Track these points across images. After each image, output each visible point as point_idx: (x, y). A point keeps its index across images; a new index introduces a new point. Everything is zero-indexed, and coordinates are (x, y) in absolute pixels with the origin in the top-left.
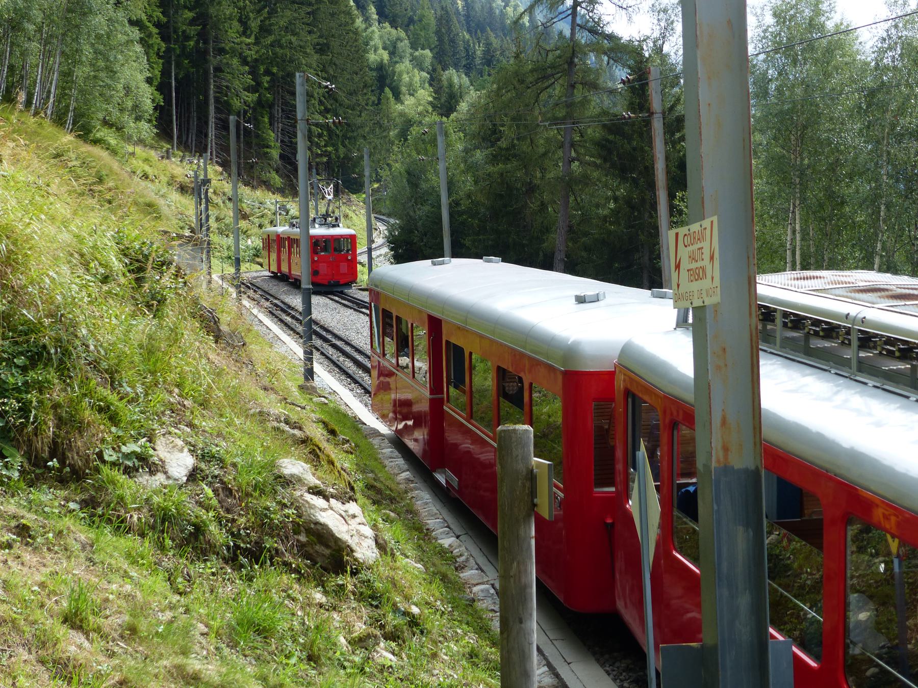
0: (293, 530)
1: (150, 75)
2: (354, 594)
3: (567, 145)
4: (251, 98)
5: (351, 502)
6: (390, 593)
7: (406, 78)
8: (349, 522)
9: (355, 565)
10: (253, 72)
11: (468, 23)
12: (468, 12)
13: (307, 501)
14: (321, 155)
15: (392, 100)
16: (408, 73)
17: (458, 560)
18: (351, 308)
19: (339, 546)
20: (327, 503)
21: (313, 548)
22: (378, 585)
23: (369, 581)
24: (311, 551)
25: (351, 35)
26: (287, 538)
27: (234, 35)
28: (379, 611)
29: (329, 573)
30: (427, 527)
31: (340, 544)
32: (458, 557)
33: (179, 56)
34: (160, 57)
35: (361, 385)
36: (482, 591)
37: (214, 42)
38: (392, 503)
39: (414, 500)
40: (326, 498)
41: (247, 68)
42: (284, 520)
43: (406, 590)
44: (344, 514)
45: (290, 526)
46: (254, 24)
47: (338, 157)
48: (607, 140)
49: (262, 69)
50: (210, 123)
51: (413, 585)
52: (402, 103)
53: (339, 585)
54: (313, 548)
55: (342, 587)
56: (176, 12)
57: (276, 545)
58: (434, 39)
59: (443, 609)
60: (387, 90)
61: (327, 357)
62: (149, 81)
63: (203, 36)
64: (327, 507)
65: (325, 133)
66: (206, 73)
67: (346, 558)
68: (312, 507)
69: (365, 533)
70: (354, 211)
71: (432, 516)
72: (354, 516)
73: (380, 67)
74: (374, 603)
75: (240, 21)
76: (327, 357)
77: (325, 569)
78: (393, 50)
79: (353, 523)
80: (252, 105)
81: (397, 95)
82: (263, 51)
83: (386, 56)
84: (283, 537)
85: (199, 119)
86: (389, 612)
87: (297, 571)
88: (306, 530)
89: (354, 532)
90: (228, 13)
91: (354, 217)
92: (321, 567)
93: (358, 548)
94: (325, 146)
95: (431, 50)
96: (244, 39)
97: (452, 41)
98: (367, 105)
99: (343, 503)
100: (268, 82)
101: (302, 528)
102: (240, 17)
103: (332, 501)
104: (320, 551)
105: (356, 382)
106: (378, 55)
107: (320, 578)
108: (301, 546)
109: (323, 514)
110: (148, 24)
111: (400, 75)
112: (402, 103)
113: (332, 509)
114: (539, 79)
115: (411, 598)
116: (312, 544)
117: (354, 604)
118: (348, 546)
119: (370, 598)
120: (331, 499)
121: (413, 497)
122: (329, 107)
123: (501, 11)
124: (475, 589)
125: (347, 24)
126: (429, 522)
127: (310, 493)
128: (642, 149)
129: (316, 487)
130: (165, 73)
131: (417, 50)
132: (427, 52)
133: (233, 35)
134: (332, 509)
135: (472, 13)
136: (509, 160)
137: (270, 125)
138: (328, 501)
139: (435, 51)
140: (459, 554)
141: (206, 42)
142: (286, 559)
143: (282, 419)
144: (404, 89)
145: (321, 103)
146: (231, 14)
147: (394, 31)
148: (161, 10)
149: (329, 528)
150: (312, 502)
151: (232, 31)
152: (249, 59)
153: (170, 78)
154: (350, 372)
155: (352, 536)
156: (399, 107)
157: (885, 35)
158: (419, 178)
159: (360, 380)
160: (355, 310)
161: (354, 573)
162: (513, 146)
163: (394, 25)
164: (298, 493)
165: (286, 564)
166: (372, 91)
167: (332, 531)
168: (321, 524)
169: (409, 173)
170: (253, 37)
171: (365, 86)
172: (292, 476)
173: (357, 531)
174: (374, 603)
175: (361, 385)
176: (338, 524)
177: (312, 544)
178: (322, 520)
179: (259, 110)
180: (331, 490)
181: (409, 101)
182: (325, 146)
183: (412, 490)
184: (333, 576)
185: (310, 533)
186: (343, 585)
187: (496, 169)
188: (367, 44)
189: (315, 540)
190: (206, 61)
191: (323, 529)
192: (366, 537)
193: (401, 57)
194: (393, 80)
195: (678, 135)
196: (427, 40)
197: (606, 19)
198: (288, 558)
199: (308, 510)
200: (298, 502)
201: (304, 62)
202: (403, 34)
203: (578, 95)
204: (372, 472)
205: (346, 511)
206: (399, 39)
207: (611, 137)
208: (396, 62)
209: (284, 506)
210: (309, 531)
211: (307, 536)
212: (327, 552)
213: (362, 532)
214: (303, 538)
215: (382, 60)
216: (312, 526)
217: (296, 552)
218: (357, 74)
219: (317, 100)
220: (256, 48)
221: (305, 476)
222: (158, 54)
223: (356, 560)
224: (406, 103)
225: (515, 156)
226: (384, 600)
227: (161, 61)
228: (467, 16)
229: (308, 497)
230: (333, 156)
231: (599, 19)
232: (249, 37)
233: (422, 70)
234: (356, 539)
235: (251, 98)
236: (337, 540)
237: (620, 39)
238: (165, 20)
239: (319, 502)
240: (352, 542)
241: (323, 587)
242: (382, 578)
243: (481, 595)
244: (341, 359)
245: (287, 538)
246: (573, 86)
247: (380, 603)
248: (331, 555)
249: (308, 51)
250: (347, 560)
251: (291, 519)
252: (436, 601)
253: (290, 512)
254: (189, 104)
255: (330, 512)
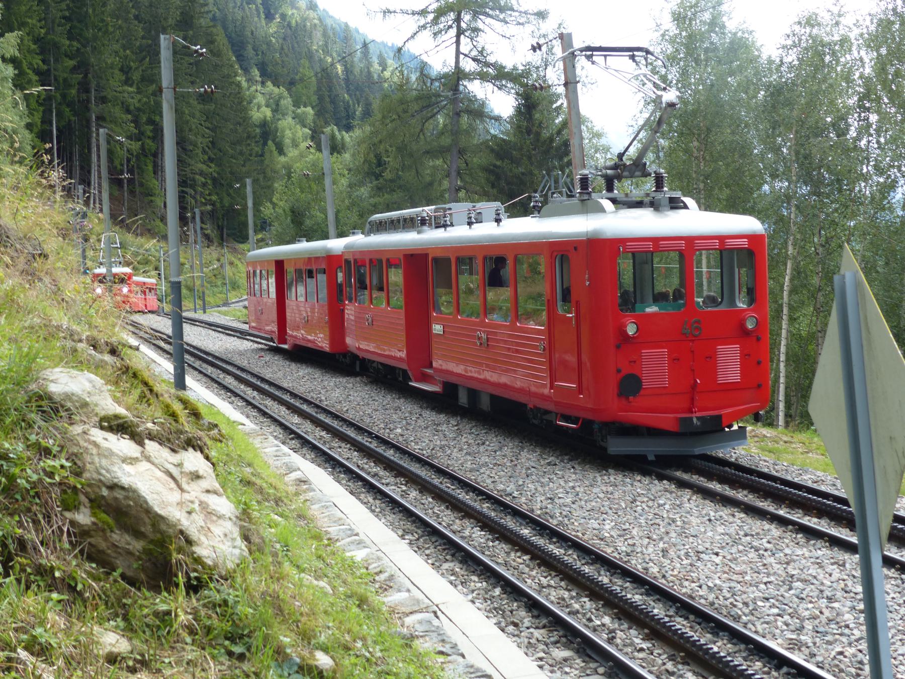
0: (63, 501)
1: (29, 121)
2: (192, 632)
3: (454, 174)
4: (135, 146)
5: (191, 450)
6: (269, 626)
7: (288, 133)
8: (185, 486)
9: (195, 570)
10: (136, 121)
11: (347, 86)
12: (347, 76)
13: (95, 444)
14: (205, 204)
15: (275, 153)
16: (290, 129)
17: (377, 578)
18: (234, 336)
19: (162, 533)
20: (139, 448)
21: (106, 539)
22: (245, 610)
23: (225, 602)
24: (103, 545)
25: (234, 86)
26: (48, 517)
27: (116, 84)
28: (246, 666)
29: (139, 589)
30: (328, 536)
31: (163, 527)
32: (377, 574)
33: (60, 104)
34: (40, 104)
35: (242, 398)
36: (420, 622)
37: (96, 90)
38: (277, 505)
39: (308, 503)
40: (137, 438)
41: (129, 117)
42: (40, 480)
43: (304, 619)
44: (175, 471)
45: (56, 493)
46: (136, 76)
47: (223, 207)
48: (495, 166)
49: (144, 119)
50: (93, 171)
51: (316, 609)
52: (285, 154)
53: (156, 614)
54: (106, 539)
55: (165, 617)
56: (56, 60)
57: (19, 531)
58: (314, 98)
59: (367, 654)
60: (270, 143)
61: (206, 375)
62: (29, 126)
63: (84, 87)
64: (138, 455)
65: (209, 181)
66: (88, 121)
67: (175, 557)
68: (109, 454)
69: (218, 509)
70: (240, 259)
71: (335, 522)
72: (196, 476)
73: (264, 124)
74: (238, 649)
75: (121, 70)
76: (206, 375)
77: (132, 582)
78: (276, 109)
79: (195, 491)
80: (135, 154)
81: (281, 151)
82: (145, 99)
83: (268, 113)
84: (40, 517)
85: (82, 168)
86: (269, 667)
87: (69, 586)
88: (91, 501)
89: (196, 506)
90: (109, 61)
91: (240, 265)
92: (123, 576)
93: (203, 538)
94: (210, 195)
95: (313, 108)
96: (126, 88)
97: (333, 102)
98: (251, 155)
99: (173, 451)
100: (151, 131)
101: (82, 498)
102: (122, 67)
103: (152, 446)
104: (122, 544)
105: (236, 395)
106: (260, 112)
107: (119, 600)
108: (80, 534)
109: (127, 468)
110: (28, 71)
111: (283, 131)
112: (285, 154)
113: (148, 459)
114: (423, 107)
115: (315, 637)
116: (103, 530)
117: (192, 653)
118: (182, 532)
119: (227, 638)
120: (147, 441)
121: (307, 500)
122: (213, 156)
123: (379, 76)
124: (409, 620)
125: (229, 76)
126: (329, 529)
127: (102, 428)
128: (531, 173)
129: (117, 417)
130: (46, 121)
131: (299, 108)
132: (309, 110)
133: (115, 84)
134: (148, 459)
135: (351, 77)
136: (394, 191)
137: (154, 173)
138: (141, 444)
139: (316, 109)
140: (378, 570)
141: (87, 91)
142: (44, 562)
143: (84, 337)
144: (287, 141)
145: (204, 152)
146: (112, 64)
147: (276, 90)
148: (40, 57)
149: (139, 496)
150: (105, 444)
151: (115, 81)
152: (132, 108)
153: (51, 125)
154: (231, 387)
155: (189, 513)
156: (282, 159)
157: (789, 32)
158: (303, 215)
159: (242, 394)
160: (238, 337)
161: (194, 588)
162: (399, 178)
163: (276, 84)
164: (77, 429)
165: (44, 572)
166: (256, 142)
167: (146, 502)
168: (123, 488)
169: (293, 212)
170: (135, 86)
171: (249, 137)
172: (68, 396)
173: (201, 503)
174: (238, 649)
175: (242, 398)
176: (160, 488)
177: (103, 530)
178: (125, 481)
179: (143, 158)
180: (150, 425)
181: (292, 153)
182: (210, 195)
183: (305, 492)
184: (148, 594)
185: (99, 507)
186: (168, 613)
187: (382, 200)
188: (250, 102)
189: (110, 520)
190: (88, 109)
191: (127, 498)
192: (219, 517)
193: (283, 115)
194: (275, 136)
195: (566, 160)
196: (309, 98)
197: (489, 48)
198: (48, 558)
199: (96, 459)
200: (78, 445)
201: (187, 112)
202: (286, 94)
203: (465, 119)
204: (249, 465)
205: (179, 465)
206: (281, 97)
207: (498, 163)
208: (279, 119)
209: (46, 452)
210: (97, 503)
211: (94, 514)
212: (137, 546)
213: (212, 506)
214: (84, 517)
215: (265, 117)
216: (105, 492)
217: (67, 546)
218: (240, 124)
219: (201, 149)
220: (139, 97)
221: (95, 399)
222: (37, 101)
223: (198, 560)
224: (290, 155)
225: (400, 187)
226: (257, 641)
227: (41, 109)
228: (347, 80)
229: (98, 435)
230: (218, 205)
231: (483, 48)
232: (131, 86)
233: (305, 127)
234: (199, 519)
235: (135, 146)
236: (157, 520)
237: (504, 68)
238: (45, 67)
239: (123, 445)
240: (191, 525)
241: (125, 618)
242: (252, 597)
243: (420, 628)
244: (221, 376)
245: (48, 517)
246: (458, 114)
247: (249, 649)
248: (146, 552)
249: (191, 101)
250: (179, 562)
251: (57, 478)
252: (355, 641)
253: (57, 463)
254: (71, 154)
255: (144, 466)
